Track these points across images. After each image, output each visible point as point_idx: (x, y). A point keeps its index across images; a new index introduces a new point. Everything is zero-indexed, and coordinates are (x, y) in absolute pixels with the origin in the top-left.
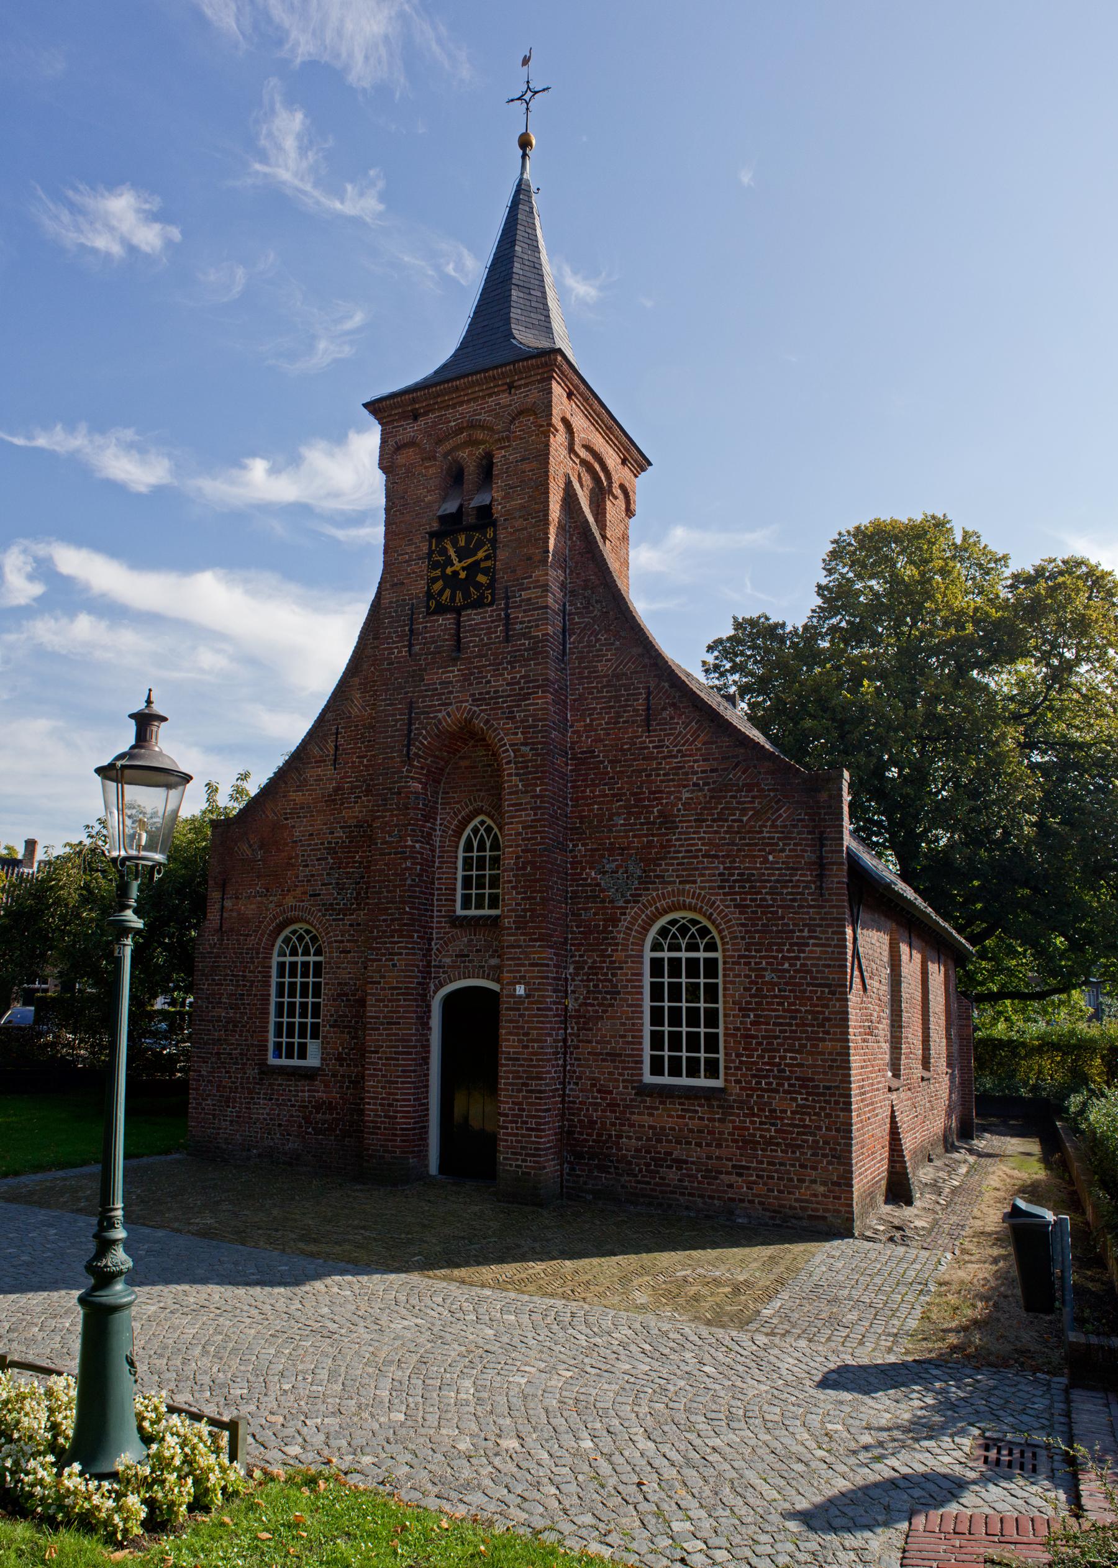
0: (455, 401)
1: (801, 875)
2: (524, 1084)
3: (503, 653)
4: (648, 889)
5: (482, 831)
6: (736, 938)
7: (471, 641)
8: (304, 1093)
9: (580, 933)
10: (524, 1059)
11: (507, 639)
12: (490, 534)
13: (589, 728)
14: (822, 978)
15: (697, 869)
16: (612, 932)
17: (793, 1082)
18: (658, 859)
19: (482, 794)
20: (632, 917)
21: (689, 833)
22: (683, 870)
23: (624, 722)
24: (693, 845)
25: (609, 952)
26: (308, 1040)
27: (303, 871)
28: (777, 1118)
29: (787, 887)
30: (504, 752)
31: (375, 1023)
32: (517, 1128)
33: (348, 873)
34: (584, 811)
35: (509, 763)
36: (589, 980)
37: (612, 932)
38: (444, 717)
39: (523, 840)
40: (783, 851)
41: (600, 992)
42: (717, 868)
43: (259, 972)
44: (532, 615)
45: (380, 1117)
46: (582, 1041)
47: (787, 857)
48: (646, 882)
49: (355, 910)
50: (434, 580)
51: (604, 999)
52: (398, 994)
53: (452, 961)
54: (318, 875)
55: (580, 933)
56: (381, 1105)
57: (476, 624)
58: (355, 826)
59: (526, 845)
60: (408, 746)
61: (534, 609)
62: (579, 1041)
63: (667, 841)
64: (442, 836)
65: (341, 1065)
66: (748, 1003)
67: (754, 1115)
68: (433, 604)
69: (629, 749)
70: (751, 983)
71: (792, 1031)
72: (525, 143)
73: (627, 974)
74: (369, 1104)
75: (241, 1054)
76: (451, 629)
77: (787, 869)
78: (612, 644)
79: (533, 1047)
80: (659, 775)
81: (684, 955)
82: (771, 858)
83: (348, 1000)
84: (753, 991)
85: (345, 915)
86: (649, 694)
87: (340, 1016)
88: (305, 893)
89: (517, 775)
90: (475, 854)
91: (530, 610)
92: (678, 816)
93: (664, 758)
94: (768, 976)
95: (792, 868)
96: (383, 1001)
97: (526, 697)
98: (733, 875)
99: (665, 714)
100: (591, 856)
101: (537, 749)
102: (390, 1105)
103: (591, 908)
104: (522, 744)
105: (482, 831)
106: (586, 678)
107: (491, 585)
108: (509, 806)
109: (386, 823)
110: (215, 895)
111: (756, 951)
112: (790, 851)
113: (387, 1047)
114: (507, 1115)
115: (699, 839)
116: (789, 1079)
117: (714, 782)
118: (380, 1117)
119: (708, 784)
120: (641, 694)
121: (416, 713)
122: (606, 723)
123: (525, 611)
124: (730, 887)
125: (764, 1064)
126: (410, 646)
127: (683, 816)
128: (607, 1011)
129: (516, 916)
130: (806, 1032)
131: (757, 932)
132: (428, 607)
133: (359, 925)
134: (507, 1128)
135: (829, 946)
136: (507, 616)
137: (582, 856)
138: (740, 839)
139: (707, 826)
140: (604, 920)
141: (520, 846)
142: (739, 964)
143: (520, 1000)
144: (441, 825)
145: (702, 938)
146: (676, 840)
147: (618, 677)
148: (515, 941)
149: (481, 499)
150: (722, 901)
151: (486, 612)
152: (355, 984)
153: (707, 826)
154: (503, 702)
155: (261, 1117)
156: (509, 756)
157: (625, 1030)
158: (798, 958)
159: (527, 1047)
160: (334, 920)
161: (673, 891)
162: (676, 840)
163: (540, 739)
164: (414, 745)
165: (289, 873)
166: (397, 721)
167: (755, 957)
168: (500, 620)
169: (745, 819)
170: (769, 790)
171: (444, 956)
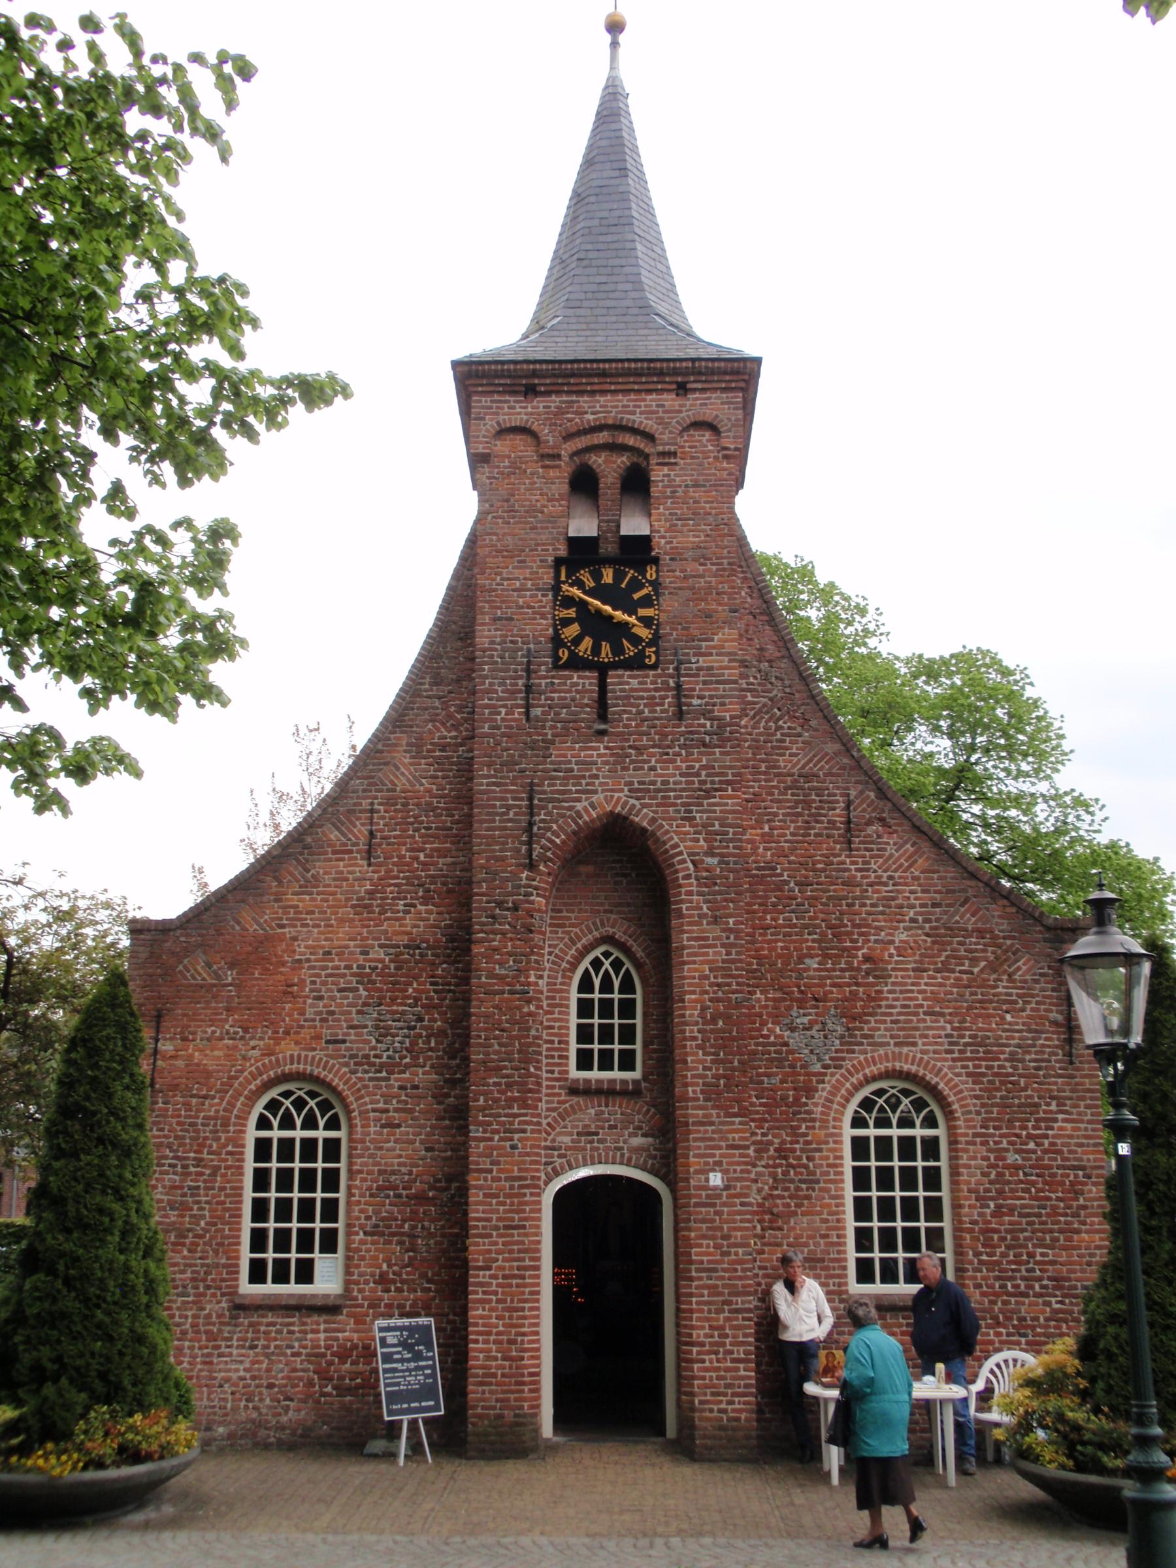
0: (596, 388)
1: (1046, 1039)
2: (724, 1303)
3: (672, 733)
4: (853, 1052)
5: (607, 964)
6: (970, 1112)
7: (625, 712)
8: (319, 1333)
9: (761, 1105)
10: (724, 1270)
11: (680, 715)
12: (651, 573)
13: (767, 838)
14: (1076, 1159)
15: (917, 1029)
16: (806, 1104)
17: (1045, 1282)
18: (866, 1014)
19: (613, 916)
20: (833, 1087)
21: (906, 984)
22: (900, 1029)
23: (816, 835)
24: (911, 999)
25: (803, 1130)
26: (316, 1255)
27: (312, 1006)
28: (1027, 1327)
29: (1029, 1053)
30: (680, 862)
31: (484, 1227)
32: (718, 1361)
33: (396, 1012)
34: (763, 949)
35: (688, 877)
36: (775, 1166)
37: (806, 1104)
38: (585, 809)
39: (711, 985)
40: (1023, 1010)
41: (792, 1181)
42: (944, 1028)
43: (228, 1153)
44: (716, 689)
45: (496, 1359)
46: (770, 1244)
47: (1028, 1017)
48: (849, 1042)
49: (407, 1066)
50: (566, 622)
51: (798, 1189)
52: (521, 1187)
53: (573, 1141)
54: (342, 1013)
55: (761, 1105)
56: (495, 1342)
57: (632, 690)
58: (405, 947)
59: (715, 992)
60: (529, 843)
61: (718, 682)
62: (764, 1244)
63: (877, 992)
64: (551, 970)
65: (388, 1291)
66: (987, 1190)
67: (998, 1324)
68: (564, 655)
69: (824, 870)
70: (991, 1166)
71: (1041, 1223)
72: (615, 27)
73: (827, 1158)
74: (476, 1341)
75: (193, 1279)
76: (592, 691)
77: (1030, 1031)
78: (800, 735)
79: (736, 1254)
80: (864, 905)
81: (895, 1132)
82: (1008, 1017)
83: (396, 1196)
84: (993, 1176)
85: (390, 1072)
86: (848, 804)
87: (383, 1219)
88: (318, 1037)
89: (700, 894)
90: (596, 996)
91: (711, 683)
92: (889, 963)
93: (871, 885)
94: (1012, 1158)
95: (1036, 1031)
96: (496, 1196)
97: (708, 794)
98: (963, 1037)
99: (871, 830)
100: (775, 1008)
101: (727, 863)
102: (510, 1342)
103: (776, 1074)
104: (706, 854)
105: (607, 964)
106: (765, 773)
107: (655, 641)
108: (689, 939)
109: (495, 949)
110: (147, 1034)
111: (995, 1128)
112: (1032, 1010)
113: (504, 1260)
114: (702, 1344)
115: (919, 992)
116: (1040, 1279)
117: (937, 920)
118: (496, 1359)
119: (926, 921)
120: (838, 802)
121: (540, 800)
122: (792, 834)
123: (704, 683)
124: (960, 1052)
125: (1009, 1262)
126: (528, 707)
127: (897, 962)
128: (801, 1205)
129: (704, 1084)
130: (1058, 1222)
131: (993, 1105)
132: (556, 658)
133: (416, 1087)
134: (703, 1361)
135: (1082, 1121)
136: (678, 687)
137: (762, 1007)
138: (972, 994)
139: (930, 977)
140: (795, 1089)
141: (707, 992)
142: (974, 1143)
143: (715, 1193)
144: (550, 954)
145: (918, 1112)
146: (890, 992)
147: (808, 777)
148: (705, 1116)
149: (634, 525)
150: (950, 1068)
151: (647, 676)
152: (410, 1173)
153: (930, 977)
154: (676, 797)
155: (234, 1376)
156: (688, 869)
157: (828, 1229)
158: (1046, 1136)
159: (728, 1254)
160: (371, 1079)
161: (886, 1054)
162: (890, 992)
163: (731, 850)
164: (538, 843)
165: (288, 1006)
166: (509, 808)
167: (993, 1135)
168: (669, 689)
169: (976, 970)
170: (1004, 938)
171: (560, 1134)
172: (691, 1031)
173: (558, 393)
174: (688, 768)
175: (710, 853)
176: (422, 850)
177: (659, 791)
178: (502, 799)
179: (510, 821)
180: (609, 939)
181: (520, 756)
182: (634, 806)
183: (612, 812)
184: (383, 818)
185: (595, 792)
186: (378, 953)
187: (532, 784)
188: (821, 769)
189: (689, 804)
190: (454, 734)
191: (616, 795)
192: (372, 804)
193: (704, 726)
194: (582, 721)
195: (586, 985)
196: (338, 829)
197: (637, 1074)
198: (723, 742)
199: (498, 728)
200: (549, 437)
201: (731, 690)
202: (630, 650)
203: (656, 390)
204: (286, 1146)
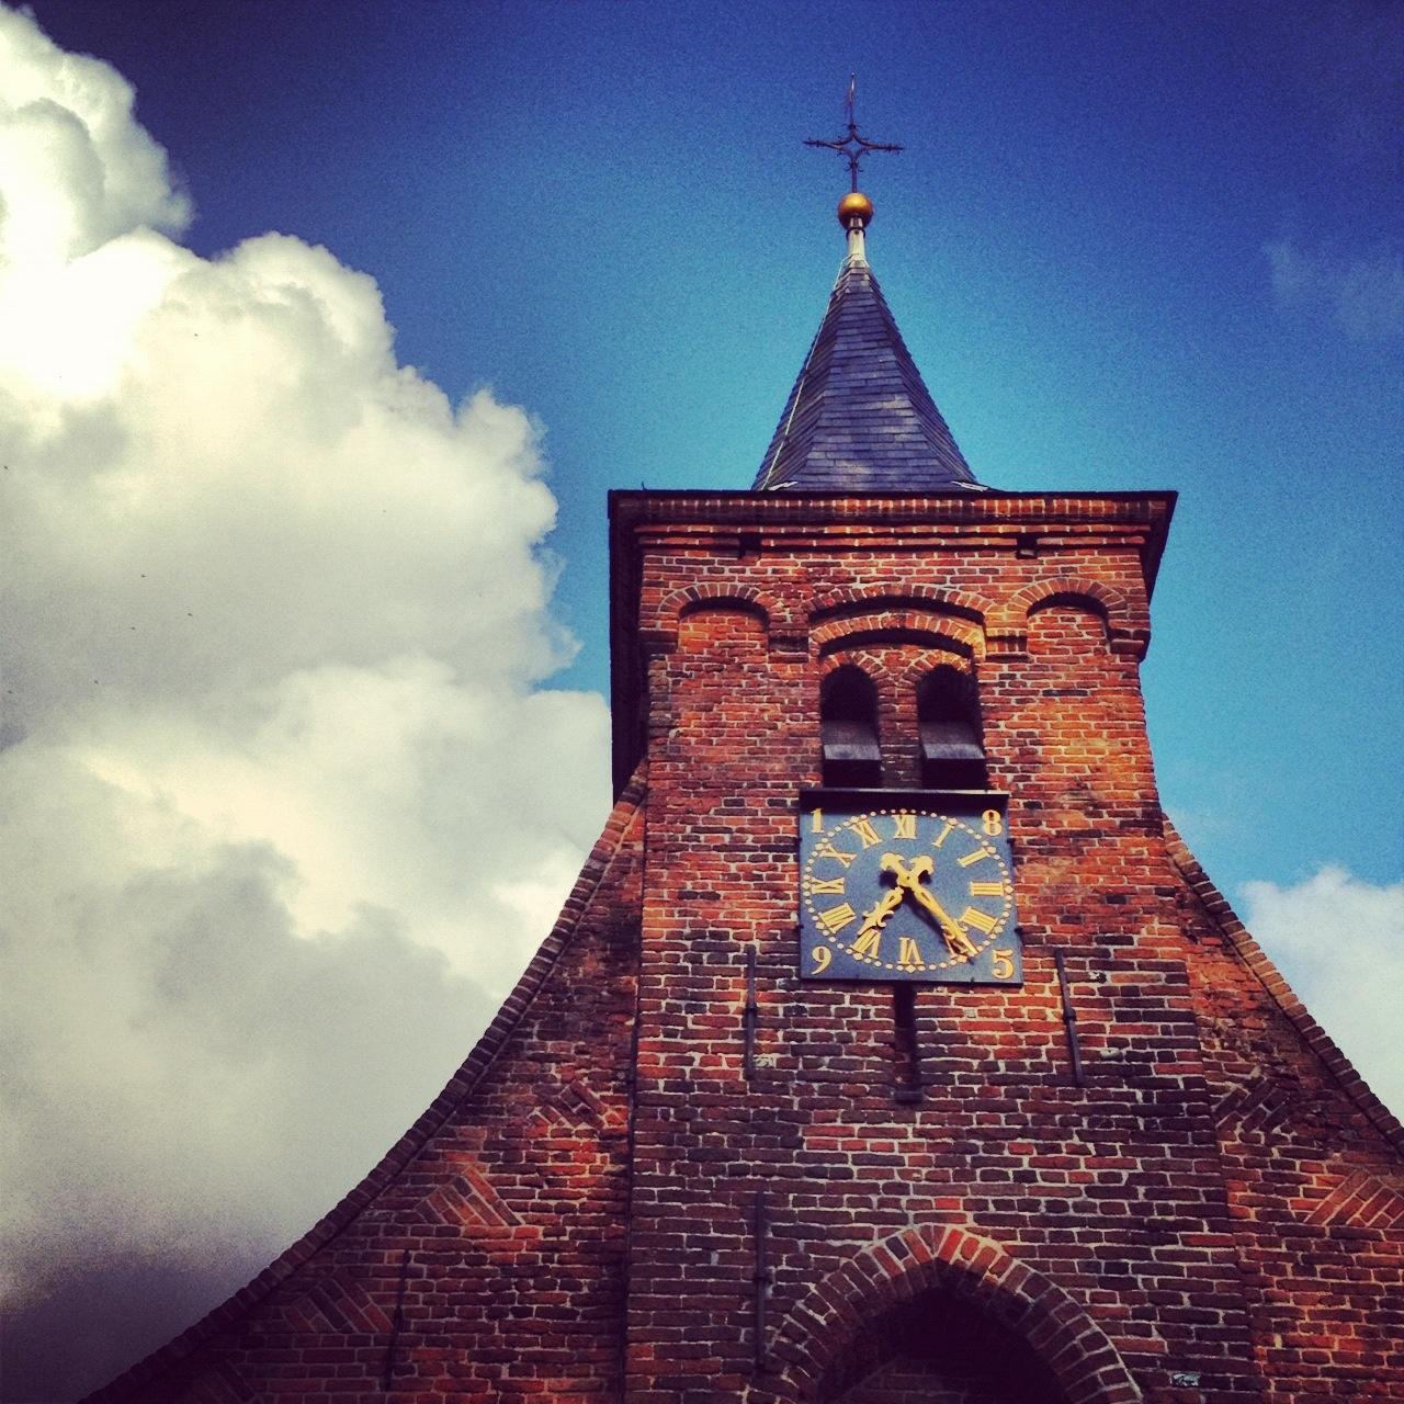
7: (956, 1066)
91: (1137, 1017)
97: (1160, 1233)
104: (1169, 1363)
173: (801, 550)
174: (1103, 1178)
176: (509, 1357)
177: (1046, 1222)
178: (692, 1227)
179: (711, 1272)
181: (735, 1142)
182: (989, 1253)
183: (941, 1263)
184: (425, 1288)
185: (903, 1220)
187: (760, 1200)
188: (1381, 1223)
189: (1118, 1253)
190: (583, 1126)
191: (949, 1228)
192: (406, 1258)
193: (1132, 1097)
194: (866, 1079)
196: (322, 1305)
199: (688, 1087)
200: (780, 608)
201: (1179, 1030)
203: (980, 548)
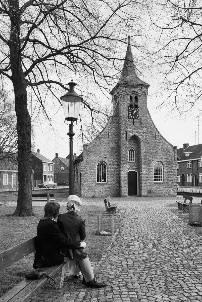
12: (138, 109)
50: (130, 114)
68: (130, 117)
107: (139, 116)
132: (129, 118)
172: (142, 157)
175: (144, 139)
180: (132, 148)
186: (109, 148)
195: (130, 152)
197: (135, 161)
198: (145, 127)
202: (136, 117)
204: (100, 168)
